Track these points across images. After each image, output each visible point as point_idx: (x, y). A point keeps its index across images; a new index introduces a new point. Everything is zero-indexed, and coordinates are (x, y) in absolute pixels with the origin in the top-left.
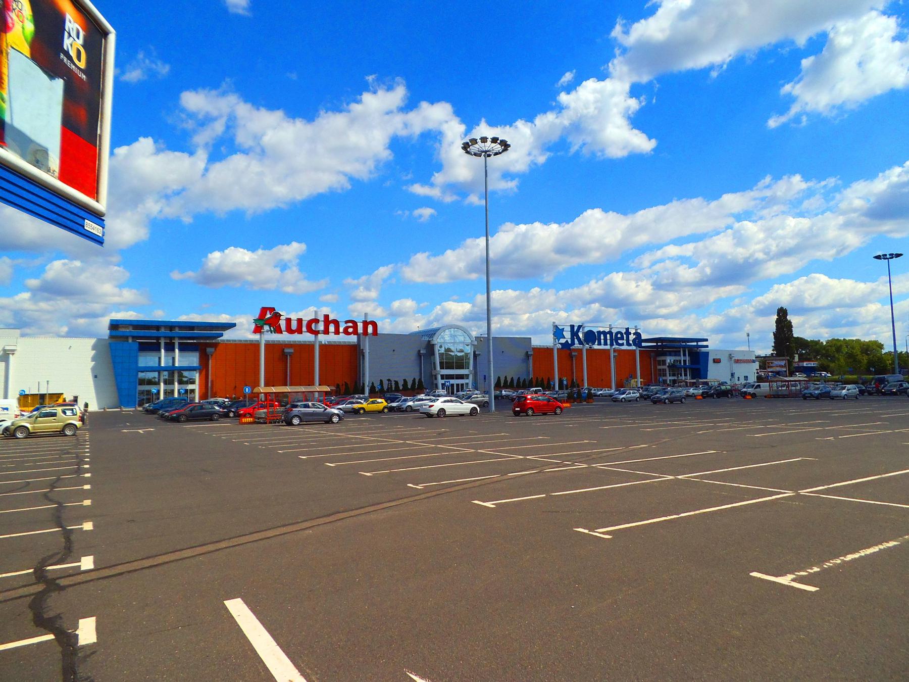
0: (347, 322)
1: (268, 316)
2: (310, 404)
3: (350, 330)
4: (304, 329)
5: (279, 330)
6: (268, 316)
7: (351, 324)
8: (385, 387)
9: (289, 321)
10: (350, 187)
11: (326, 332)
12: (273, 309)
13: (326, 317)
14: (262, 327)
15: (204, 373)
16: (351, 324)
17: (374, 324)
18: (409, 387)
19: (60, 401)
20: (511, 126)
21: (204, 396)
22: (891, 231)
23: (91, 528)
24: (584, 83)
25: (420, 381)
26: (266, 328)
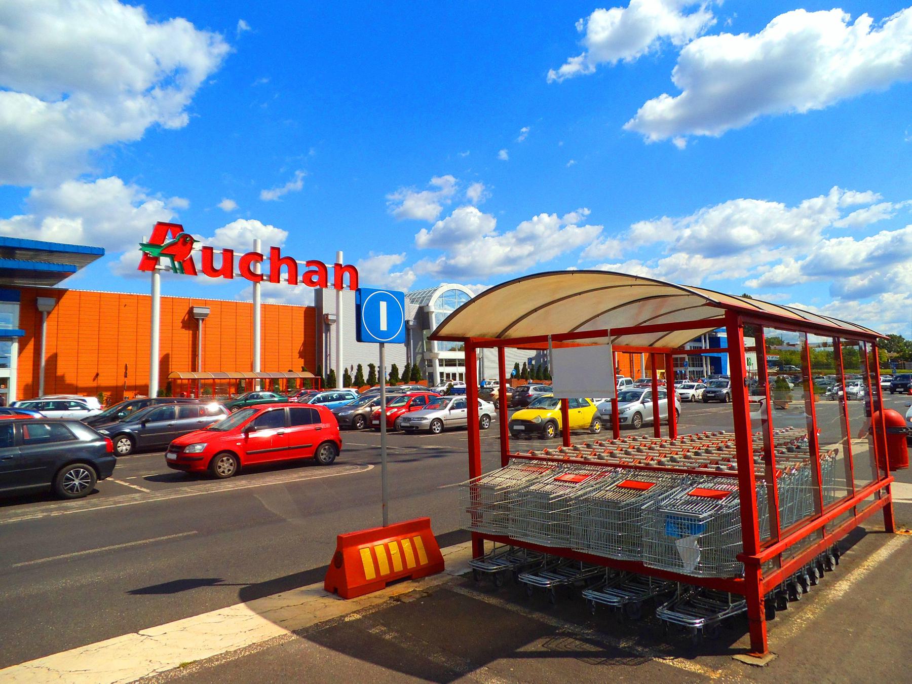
0: (309, 263)
1: (168, 240)
2: (177, 409)
3: (315, 278)
4: (236, 271)
5: (188, 268)
6: (168, 240)
7: (314, 268)
8: (366, 377)
9: (208, 252)
10: (836, 187)
11: (275, 277)
12: (180, 227)
13: (275, 251)
14: (156, 260)
15: (31, 346)
16: (314, 268)
17: (353, 270)
18: (400, 376)
19: (106, 394)
20: (607, 10)
21: (30, 391)
22: (865, 206)
23: (441, 550)
24: (775, 20)
25: (415, 365)
26: (165, 261)
